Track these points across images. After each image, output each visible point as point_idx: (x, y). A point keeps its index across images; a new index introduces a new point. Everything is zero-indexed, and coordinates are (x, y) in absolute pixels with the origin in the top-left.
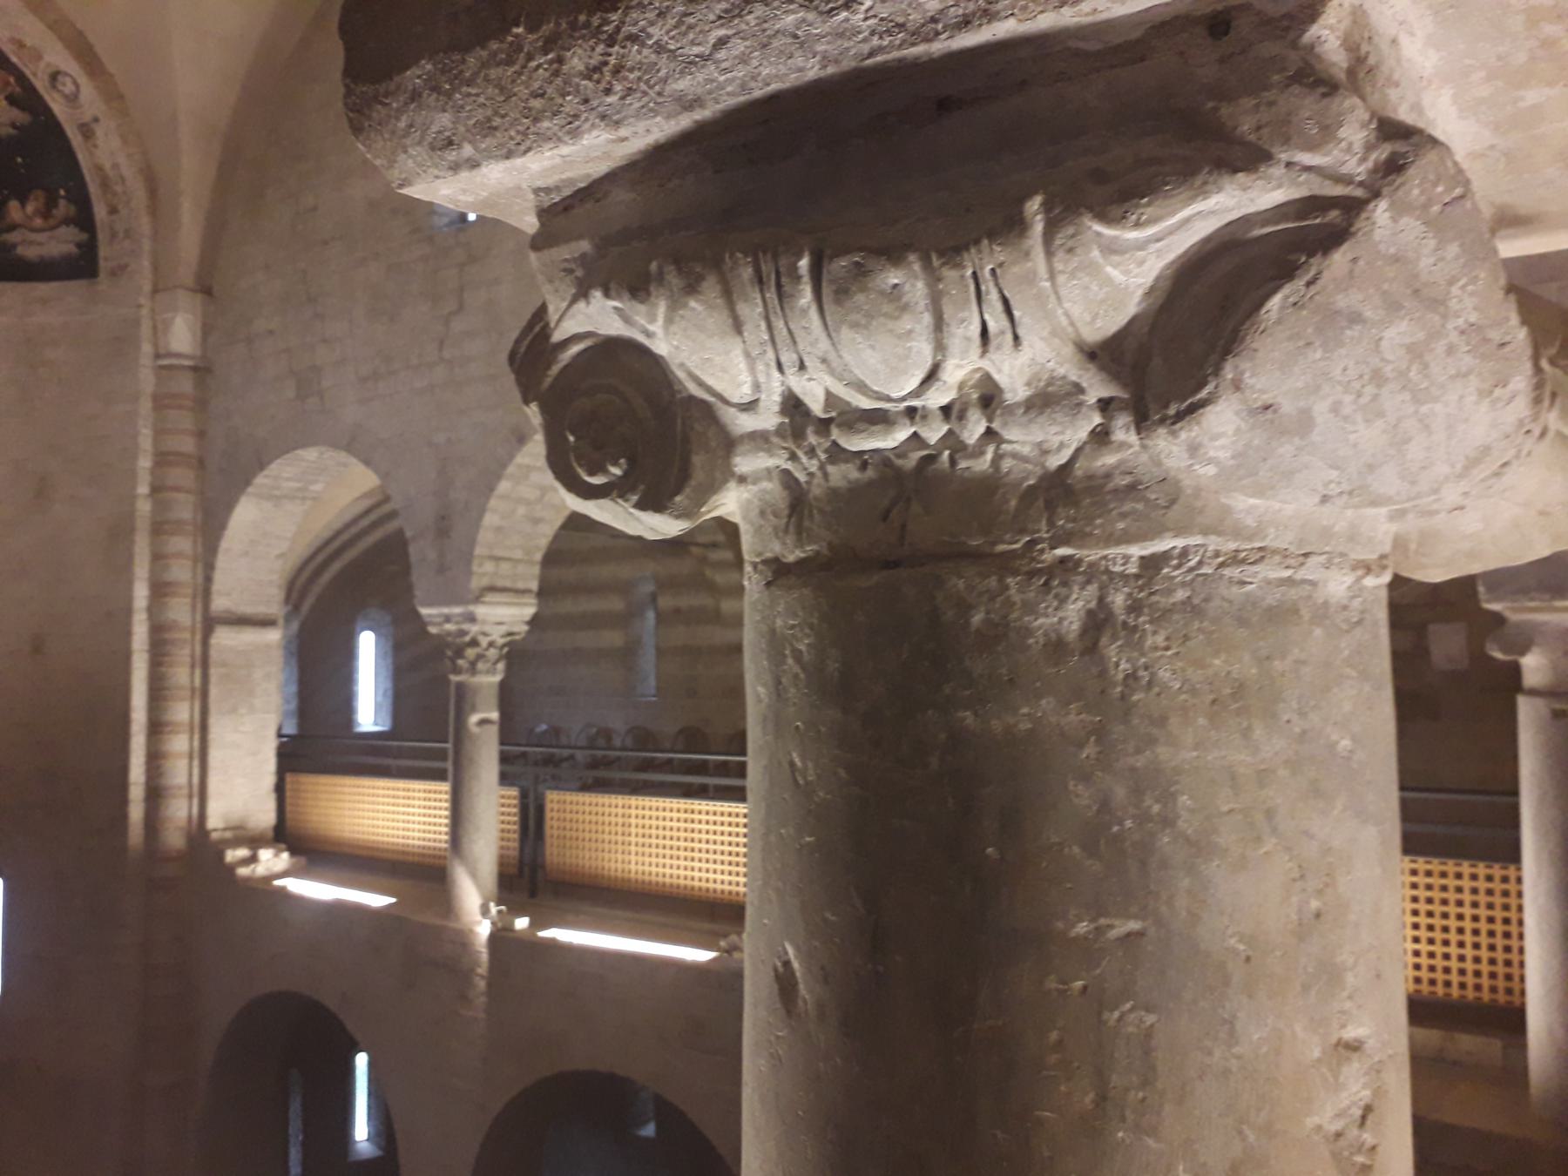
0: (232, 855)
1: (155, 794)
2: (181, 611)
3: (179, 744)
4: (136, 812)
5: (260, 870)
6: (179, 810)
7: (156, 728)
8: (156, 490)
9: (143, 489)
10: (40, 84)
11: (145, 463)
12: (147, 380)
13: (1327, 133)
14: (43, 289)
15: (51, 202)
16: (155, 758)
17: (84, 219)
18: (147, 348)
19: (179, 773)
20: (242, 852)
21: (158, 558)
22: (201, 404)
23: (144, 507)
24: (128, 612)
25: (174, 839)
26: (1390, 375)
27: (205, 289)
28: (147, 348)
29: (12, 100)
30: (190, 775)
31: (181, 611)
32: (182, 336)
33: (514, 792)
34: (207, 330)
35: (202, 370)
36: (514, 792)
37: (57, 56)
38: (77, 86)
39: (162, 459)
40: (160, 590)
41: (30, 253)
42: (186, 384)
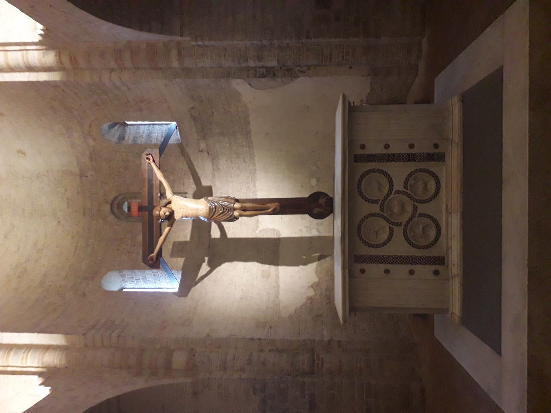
1: (30, 69)
4: (43, 77)
6: (35, 56)
30: (29, 347)
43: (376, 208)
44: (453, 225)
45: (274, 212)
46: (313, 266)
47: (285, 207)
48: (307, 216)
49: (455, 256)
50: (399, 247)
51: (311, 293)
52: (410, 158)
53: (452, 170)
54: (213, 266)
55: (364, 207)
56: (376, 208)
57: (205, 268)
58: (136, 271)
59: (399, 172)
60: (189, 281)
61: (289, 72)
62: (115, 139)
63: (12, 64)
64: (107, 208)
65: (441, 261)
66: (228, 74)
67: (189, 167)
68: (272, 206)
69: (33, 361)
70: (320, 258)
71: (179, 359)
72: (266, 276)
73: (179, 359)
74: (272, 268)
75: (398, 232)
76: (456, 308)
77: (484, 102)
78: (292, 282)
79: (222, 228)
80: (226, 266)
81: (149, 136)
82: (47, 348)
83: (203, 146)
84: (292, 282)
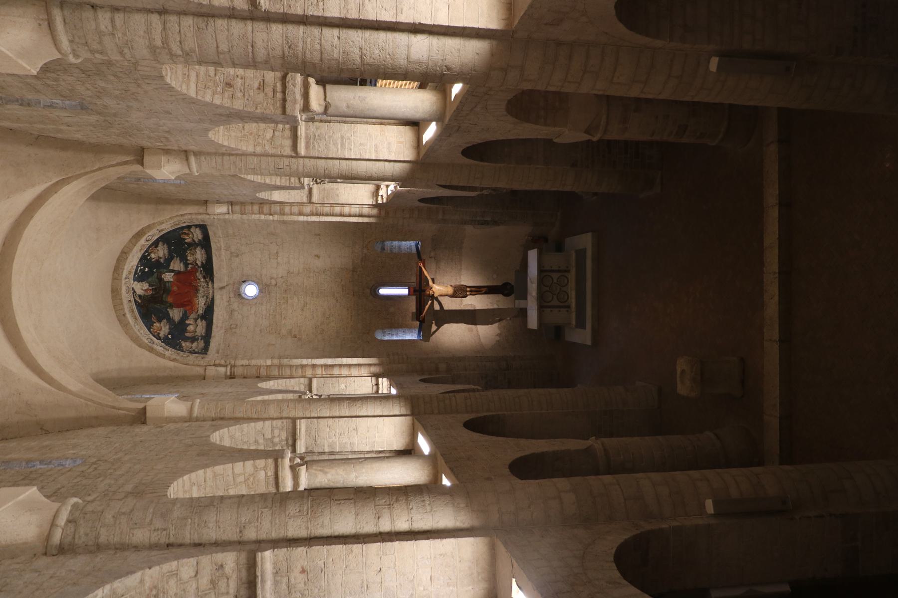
0: (380, 202)
1: (361, 216)
2: (308, 209)
3: (347, 210)
4: (366, 220)
5: (385, 196)
6: (366, 210)
7: (342, 215)
8: (271, 214)
9: (271, 218)
10: (150, 243)
11: (263, 217)
12: (237, 217)
13: (86, 60)
14: (211, 233)
15: (185, 234)
16: (350, 216)
17: (189, 227)
18: (227, 216)
19: (355, 210)
20: (380, 198)
21: (291, 214)
22: (243, 204)
23: (276, 217)
24: (320, 222)
25: (375, 212)
26: (185, 349)
27: (206, 202)
28: (227, 216)
29: (156, 247)
30: (360, 365)
31: (308, 209)
32: (223, 209)
33: (380, 81)
34: (219, 202)
35: (232, 204)
36: (380, 81)
37: (142, 241)
38: (156, 244)
39: (261, 212)
40: (300, 214)
41: (200, 237)
42: (237, 208)
43: (547, 289)
44: (573, 294)
45: (485, 293)
46: (496, 325)
47: (476, 290)
48: (501, 296)
49: (573, 305)
50: (555, 302)
51: (498, 338)
52: (559, 271)
53: (572, 276)
54: (439, 326)
55: (255, 298)
56: (547, 289)
57: (434, 328)
58: (426, 498)
59: (555, 276)
60: (426, 333)
61: (496, 223)
62: (379, 250)
63: (352, 213)
64: (368, 291)
65: (569, 307)
66: (465, 223)
67: (381, 533)
68: (484, 290)
69: (364, 371)
70: (500, 321)
71: (443, 366)
72: (471, 330)
73: (443, 366)
74: (473, 327)
75: (555, 297)
76: (574, 322)
77: (581, 254)
78: (486, 333)
79: (440, 303)
80: (446, 325)
81: (400, 248)
82: (370, 365)
83: (432, 254)
84: (486, 333)
